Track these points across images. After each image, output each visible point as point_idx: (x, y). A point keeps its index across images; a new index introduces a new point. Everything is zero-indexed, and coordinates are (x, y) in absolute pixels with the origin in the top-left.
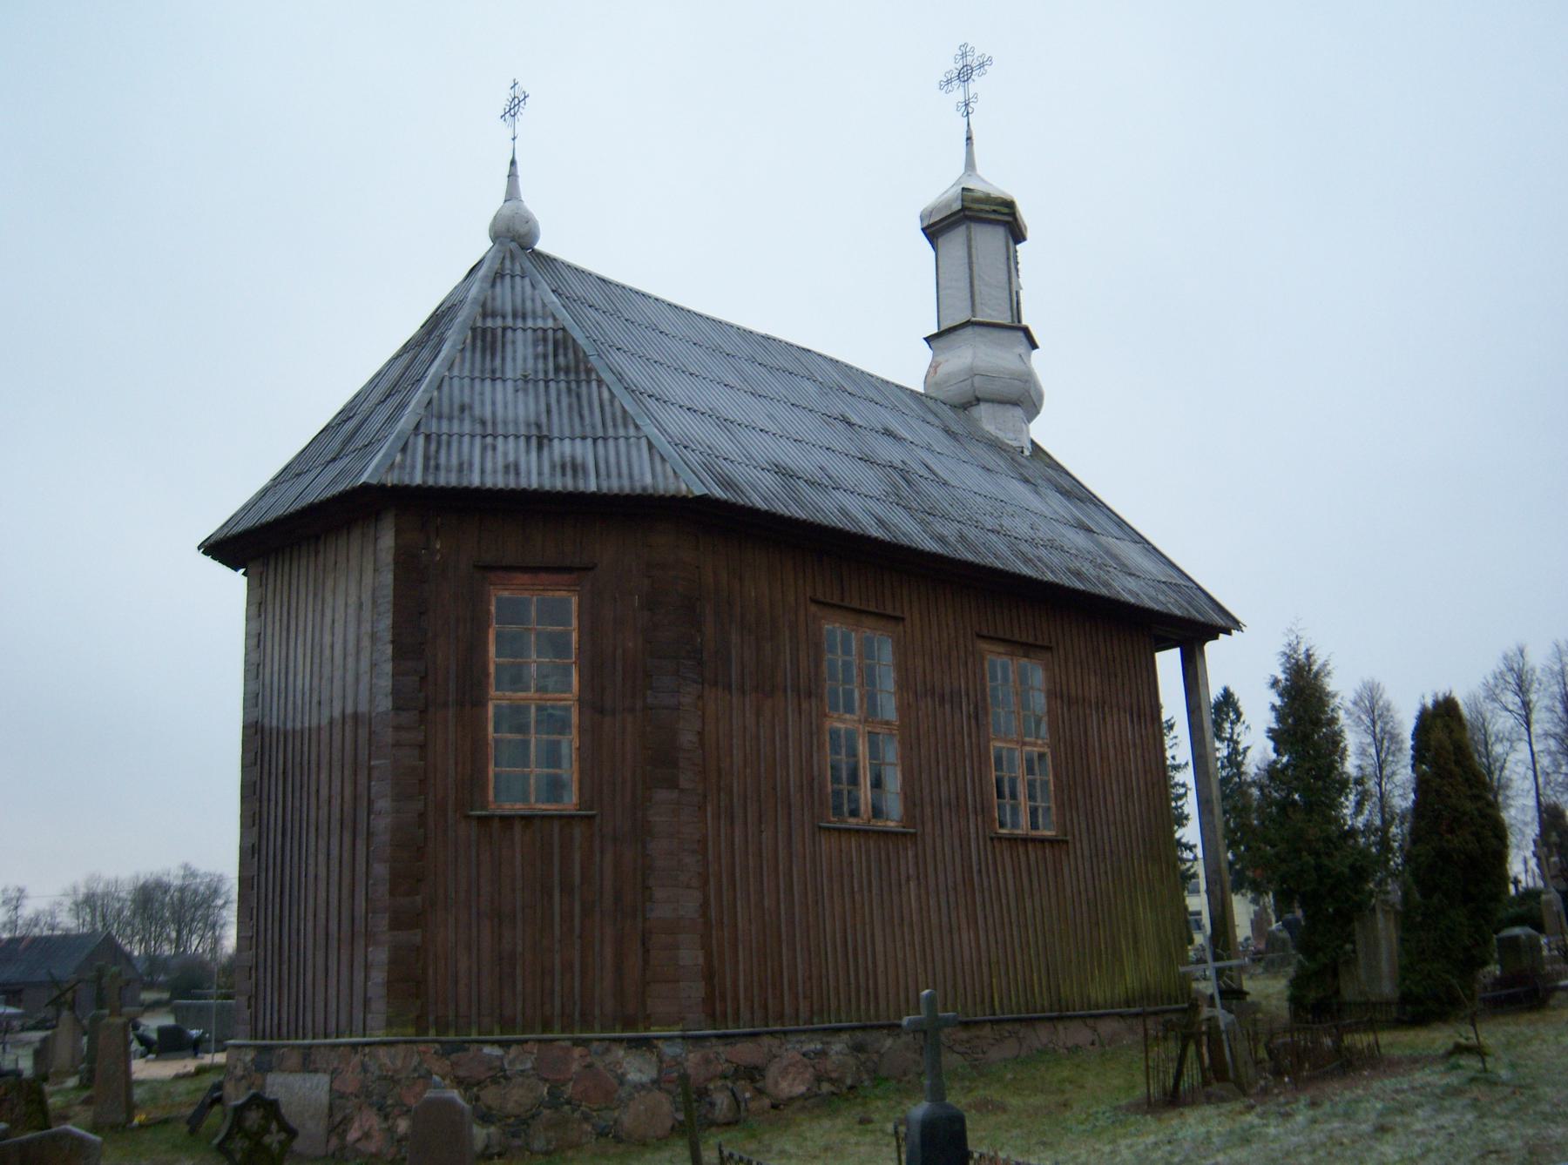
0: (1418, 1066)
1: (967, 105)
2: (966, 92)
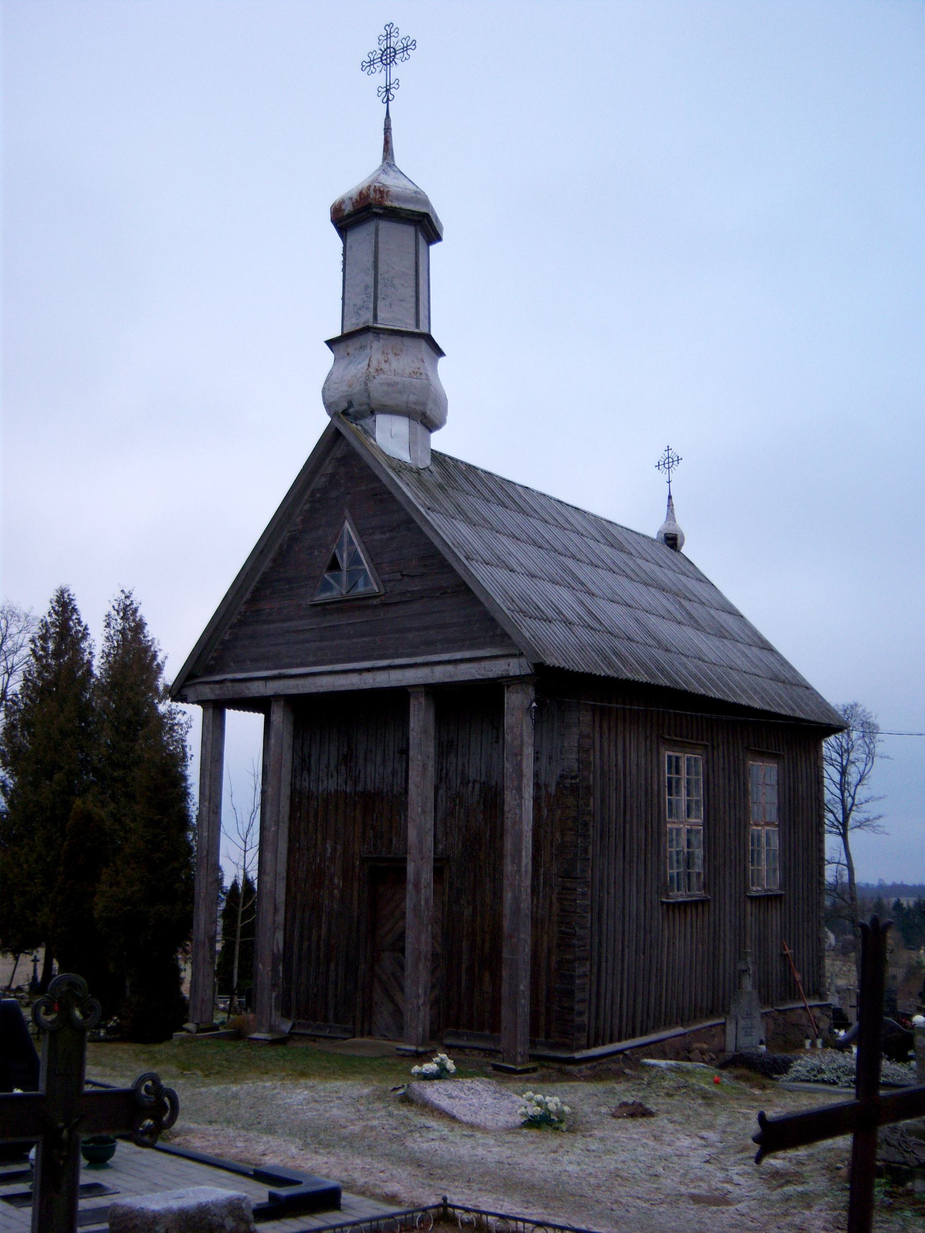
0: (290, 1077)
1: (387, 91)
2: (388, 75)
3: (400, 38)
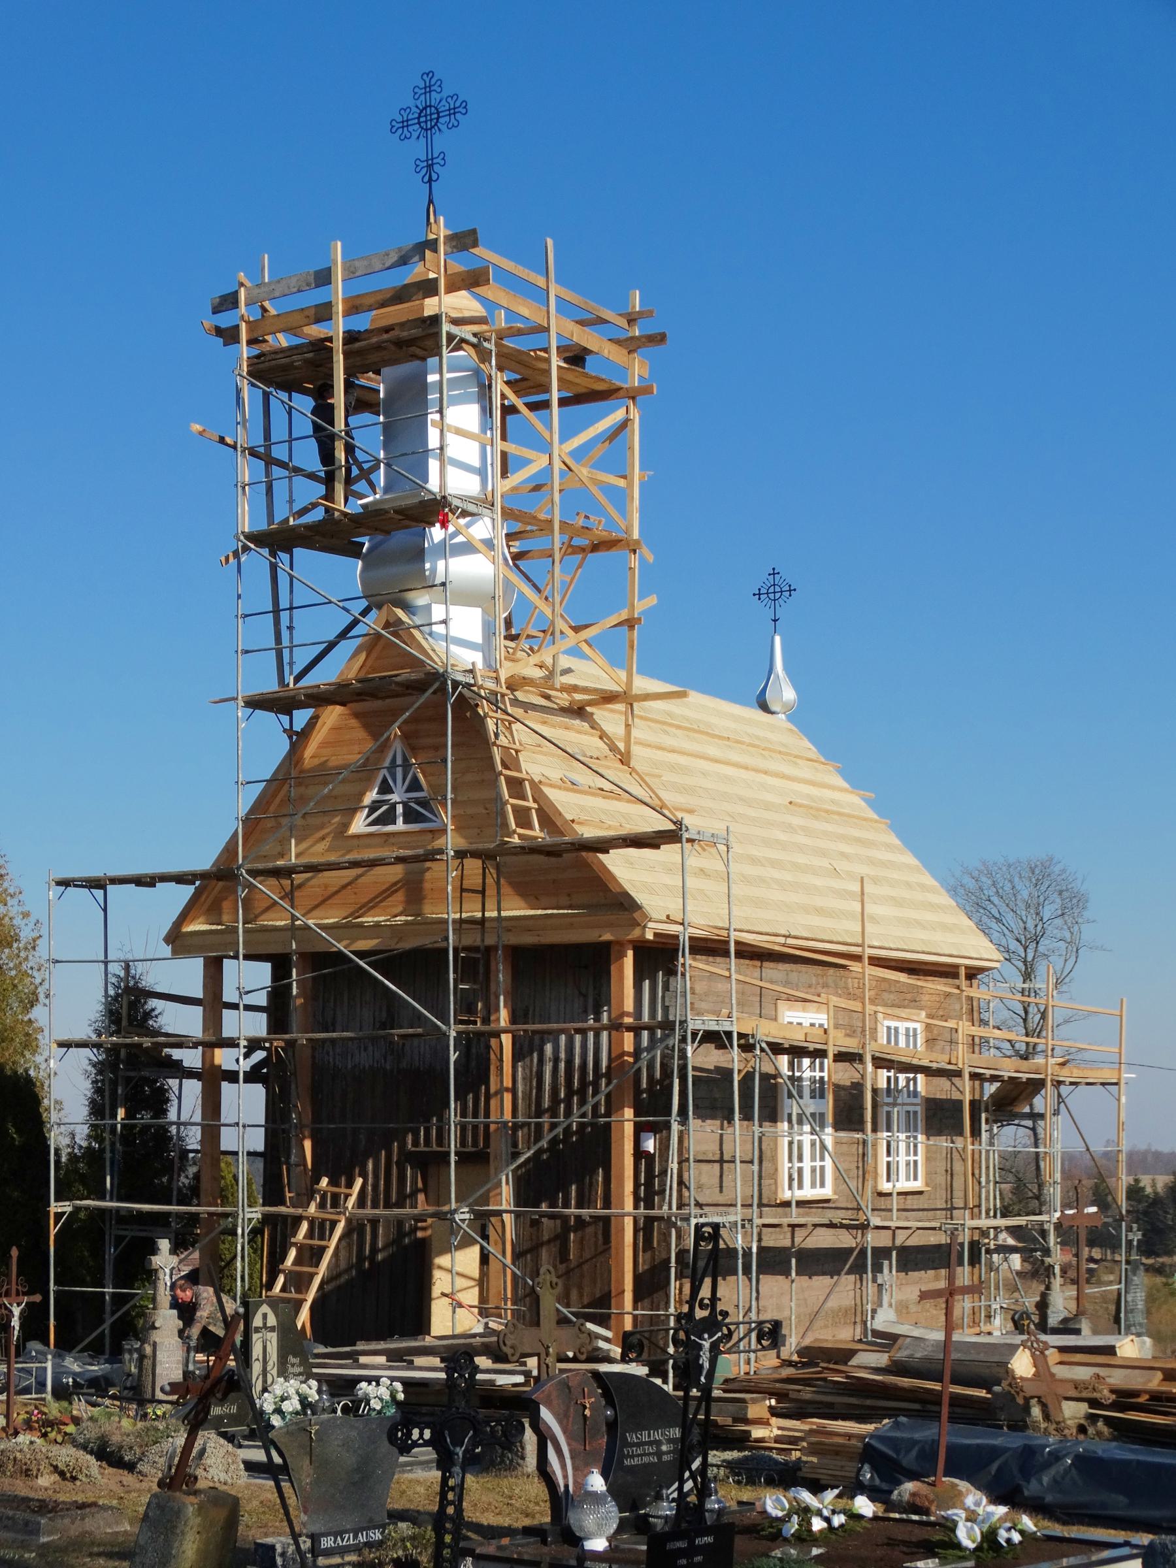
1: (430, 167)
2: (430, 145)
3: (445, 94)
